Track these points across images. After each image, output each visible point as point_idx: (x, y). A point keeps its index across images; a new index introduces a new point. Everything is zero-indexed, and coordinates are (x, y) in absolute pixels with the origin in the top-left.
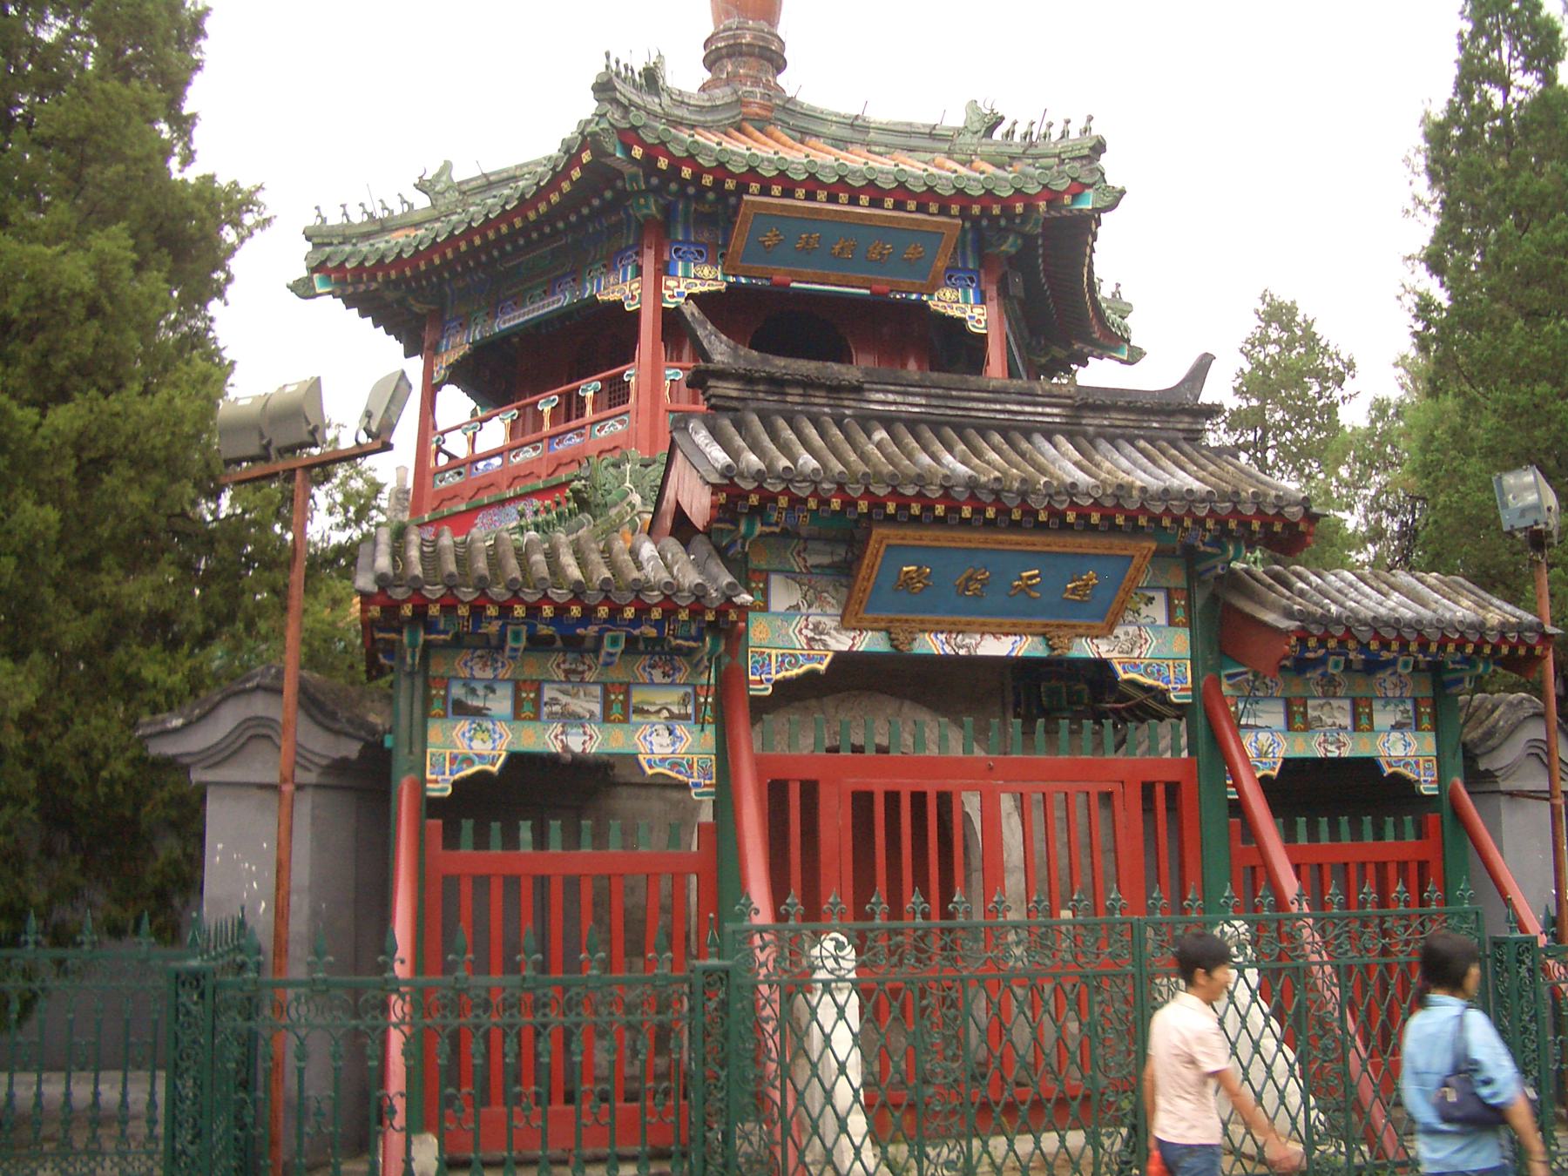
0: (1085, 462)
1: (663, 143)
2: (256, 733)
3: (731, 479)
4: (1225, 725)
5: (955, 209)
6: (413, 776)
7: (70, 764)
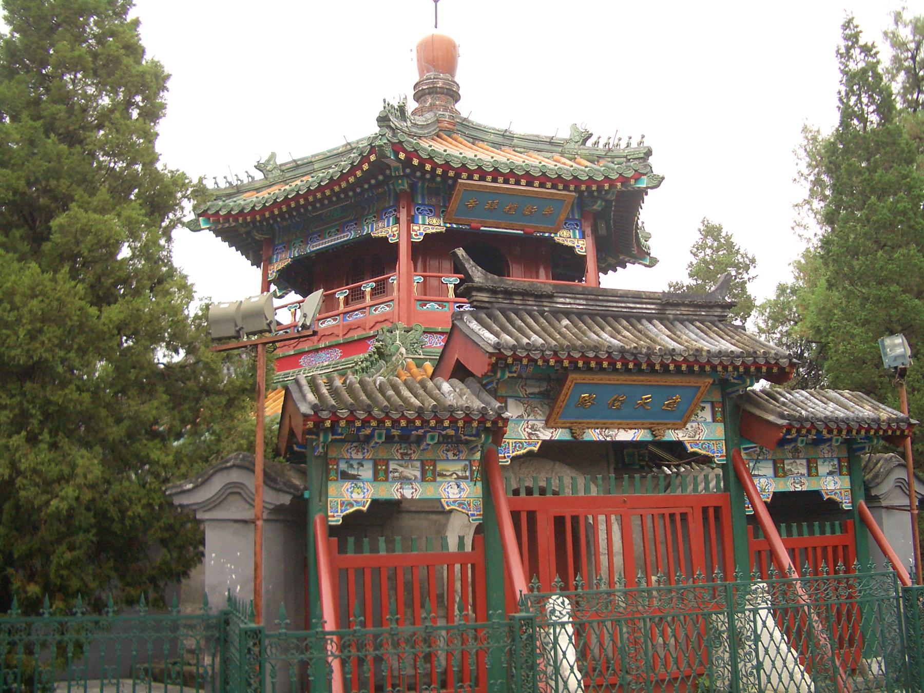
0: (673, 336)
1: (416, 151)
2: (234, 491)
3: (499, 350)
4: (745, 475)
5: (572, 187)
6: (322, 514)
7: (111, 508)
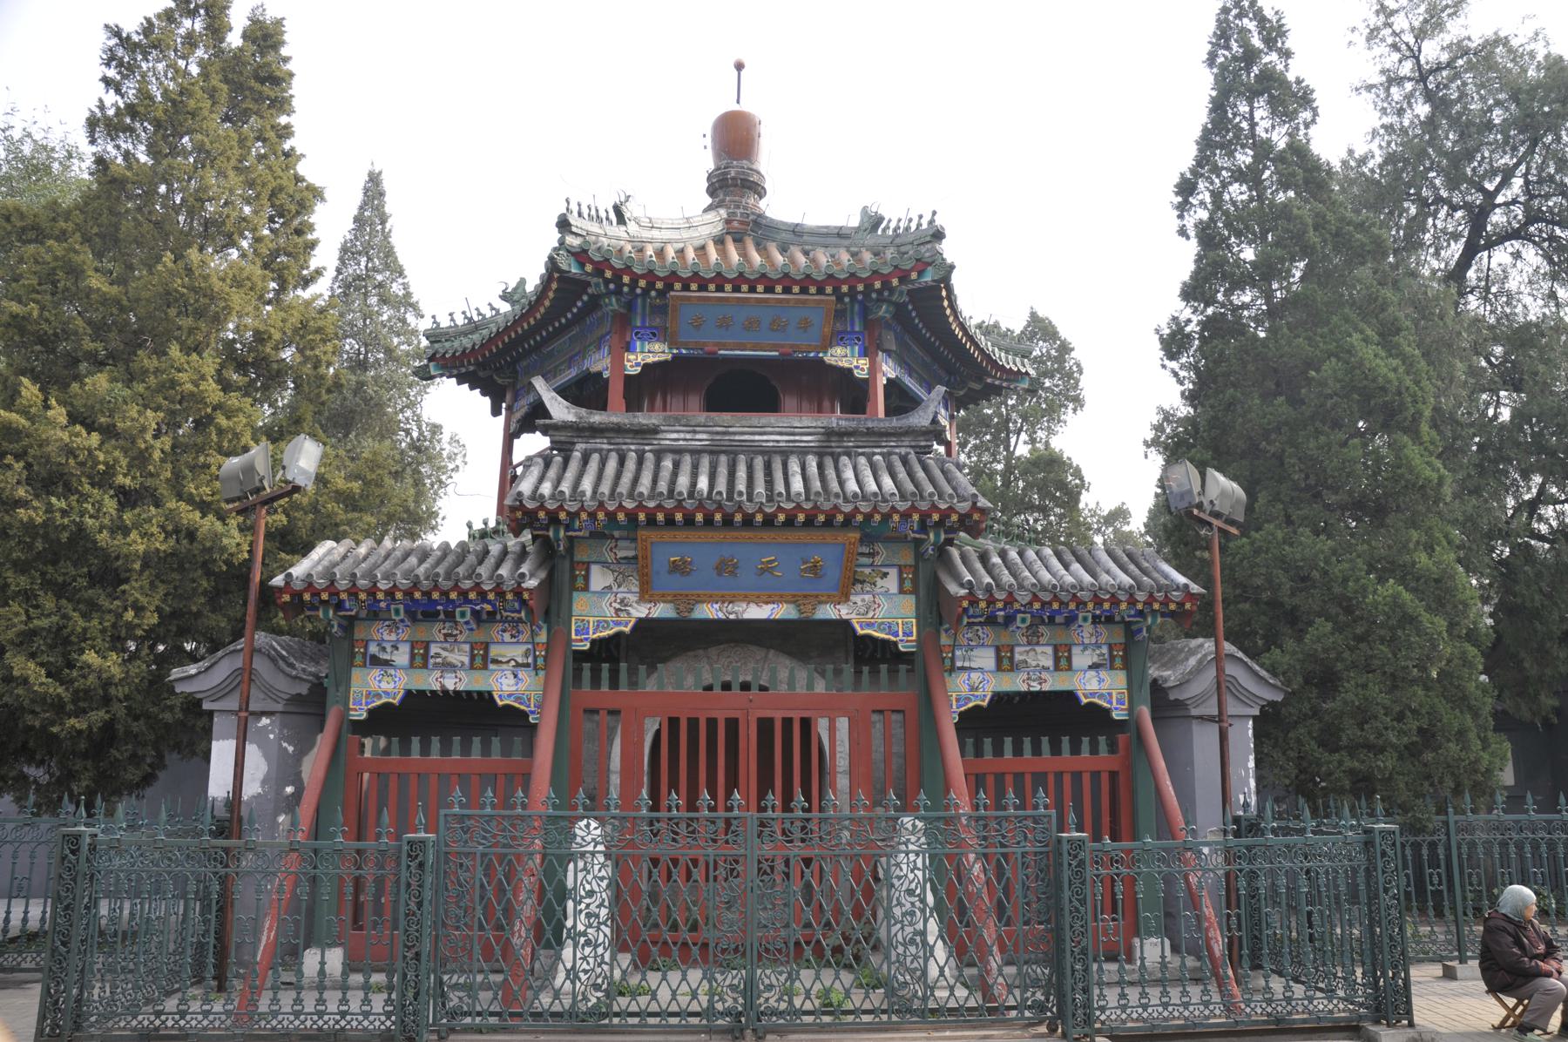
5: (829, 290)
